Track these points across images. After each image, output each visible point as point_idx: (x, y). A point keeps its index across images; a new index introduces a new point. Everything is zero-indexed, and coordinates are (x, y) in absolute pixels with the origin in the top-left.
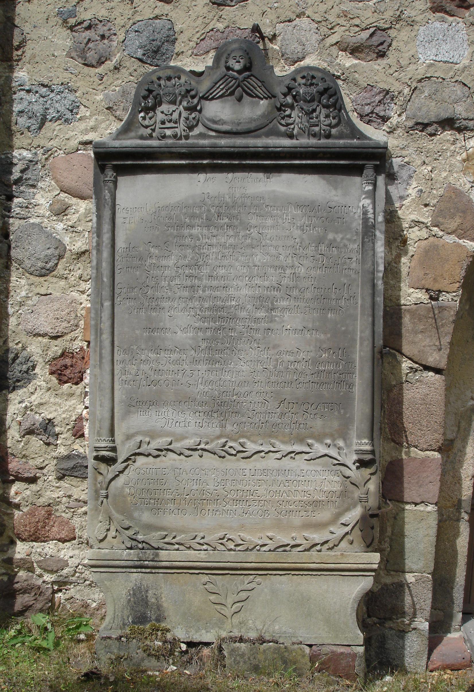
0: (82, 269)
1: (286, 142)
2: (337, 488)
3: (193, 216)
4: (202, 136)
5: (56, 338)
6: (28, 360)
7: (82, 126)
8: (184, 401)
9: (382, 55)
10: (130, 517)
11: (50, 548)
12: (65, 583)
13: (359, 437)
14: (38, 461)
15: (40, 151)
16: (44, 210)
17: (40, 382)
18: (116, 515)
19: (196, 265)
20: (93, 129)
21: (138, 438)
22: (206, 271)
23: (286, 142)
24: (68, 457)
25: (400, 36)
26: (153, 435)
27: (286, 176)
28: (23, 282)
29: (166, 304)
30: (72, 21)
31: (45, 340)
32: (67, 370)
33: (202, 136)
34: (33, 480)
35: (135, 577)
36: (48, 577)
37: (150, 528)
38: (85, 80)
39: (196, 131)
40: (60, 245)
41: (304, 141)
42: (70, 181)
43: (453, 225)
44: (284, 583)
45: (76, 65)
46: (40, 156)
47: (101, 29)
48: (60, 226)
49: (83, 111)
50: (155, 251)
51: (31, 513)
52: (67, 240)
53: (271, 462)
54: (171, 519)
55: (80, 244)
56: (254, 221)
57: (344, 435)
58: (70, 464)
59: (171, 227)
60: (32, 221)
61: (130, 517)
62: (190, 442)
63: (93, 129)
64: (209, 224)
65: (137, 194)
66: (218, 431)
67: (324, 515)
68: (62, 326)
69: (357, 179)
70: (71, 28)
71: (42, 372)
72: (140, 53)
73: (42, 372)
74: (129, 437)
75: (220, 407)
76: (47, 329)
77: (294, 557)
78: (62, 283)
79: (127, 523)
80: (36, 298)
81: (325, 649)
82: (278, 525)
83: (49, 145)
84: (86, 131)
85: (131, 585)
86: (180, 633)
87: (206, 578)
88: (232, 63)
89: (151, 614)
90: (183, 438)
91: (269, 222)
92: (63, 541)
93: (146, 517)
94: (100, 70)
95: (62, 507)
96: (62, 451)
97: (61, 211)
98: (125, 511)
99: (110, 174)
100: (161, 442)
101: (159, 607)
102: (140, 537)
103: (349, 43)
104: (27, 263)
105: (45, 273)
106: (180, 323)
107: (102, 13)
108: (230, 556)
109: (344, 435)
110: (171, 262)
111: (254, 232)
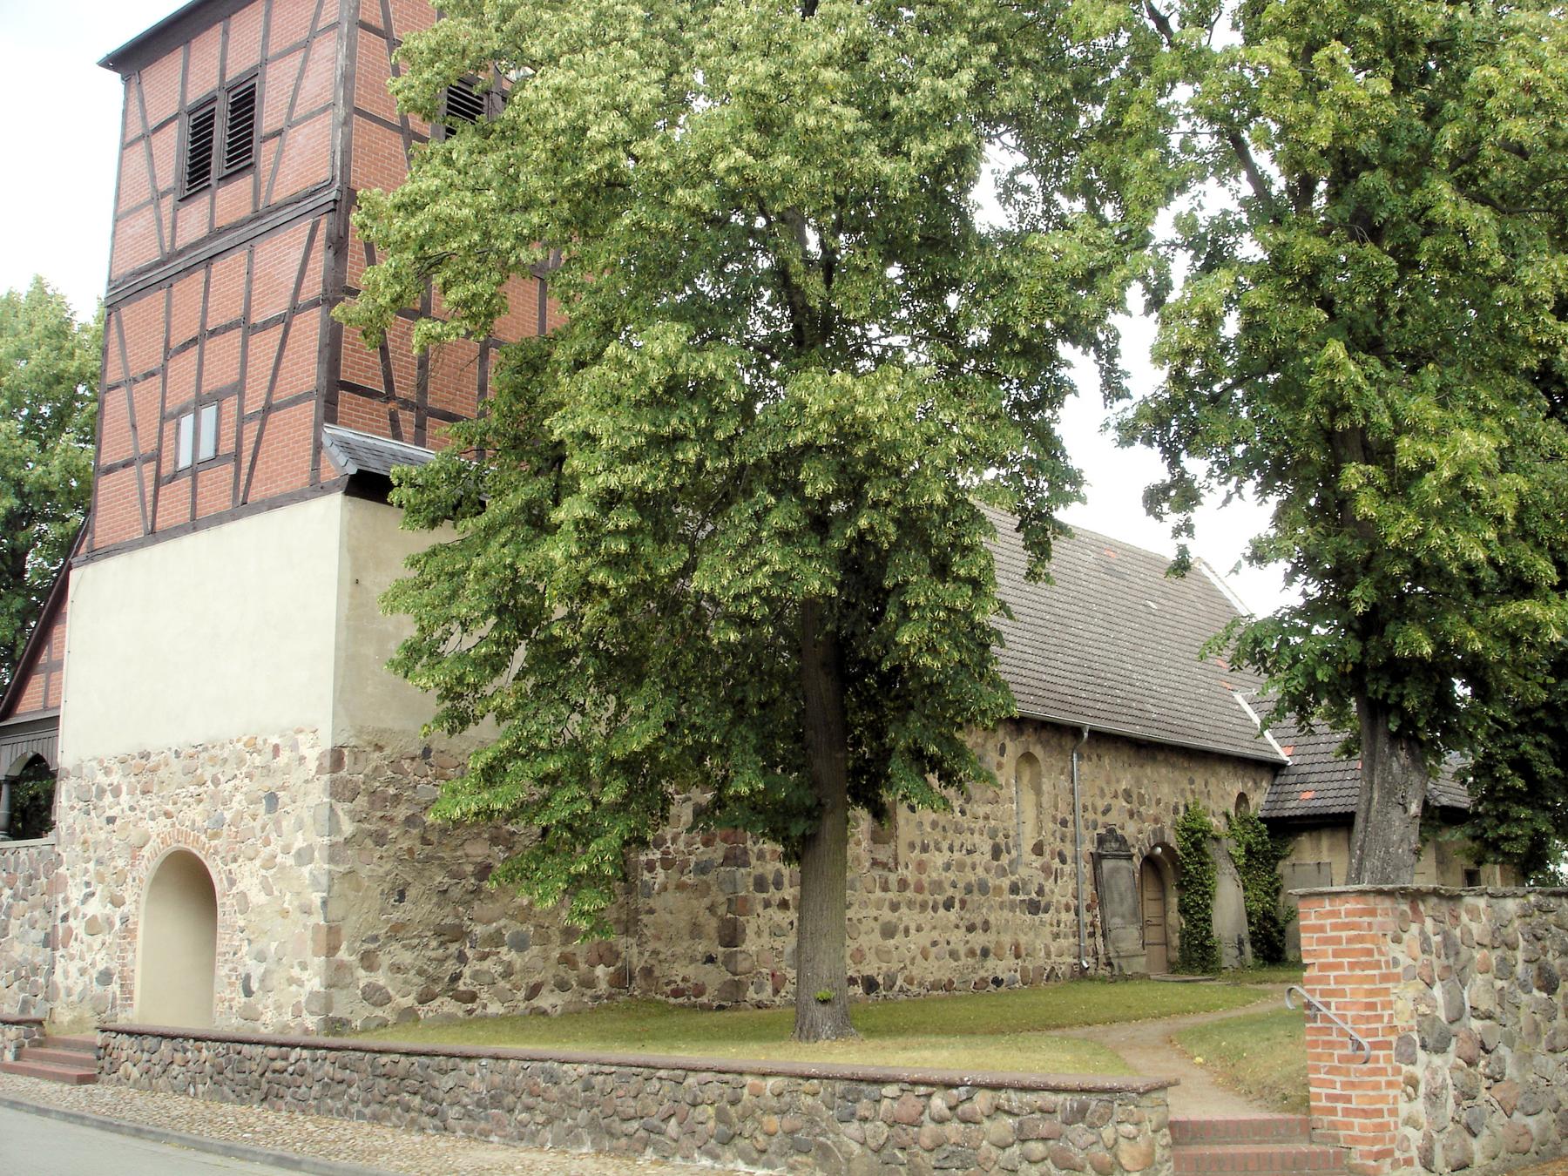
59: (1116, 870)
75: (1123, 917)
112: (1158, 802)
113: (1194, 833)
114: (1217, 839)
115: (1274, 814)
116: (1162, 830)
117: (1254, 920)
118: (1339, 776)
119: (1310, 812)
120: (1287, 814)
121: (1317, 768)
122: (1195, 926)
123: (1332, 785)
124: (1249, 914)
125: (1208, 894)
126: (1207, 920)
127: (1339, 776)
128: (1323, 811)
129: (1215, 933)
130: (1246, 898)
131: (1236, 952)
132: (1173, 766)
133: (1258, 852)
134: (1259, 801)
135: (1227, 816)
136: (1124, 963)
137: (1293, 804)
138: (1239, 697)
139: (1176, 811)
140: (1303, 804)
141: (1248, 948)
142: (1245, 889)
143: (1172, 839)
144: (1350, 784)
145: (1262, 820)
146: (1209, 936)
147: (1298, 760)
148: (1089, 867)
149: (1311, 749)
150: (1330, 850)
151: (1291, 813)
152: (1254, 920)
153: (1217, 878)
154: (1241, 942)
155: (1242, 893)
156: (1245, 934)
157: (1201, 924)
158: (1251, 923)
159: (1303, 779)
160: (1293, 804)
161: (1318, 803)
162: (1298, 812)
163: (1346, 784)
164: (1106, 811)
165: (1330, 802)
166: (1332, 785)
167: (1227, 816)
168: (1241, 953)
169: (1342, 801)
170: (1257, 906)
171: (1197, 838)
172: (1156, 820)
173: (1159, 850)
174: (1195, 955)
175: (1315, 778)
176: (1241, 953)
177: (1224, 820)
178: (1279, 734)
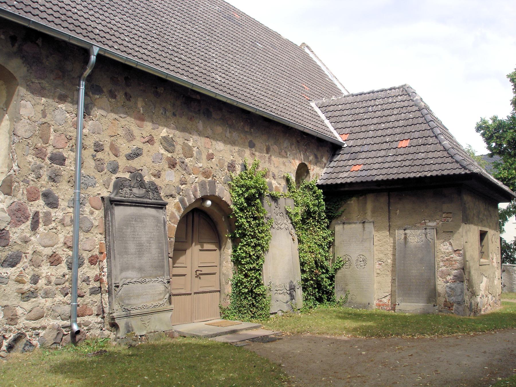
0: (96, 231)
1: (150, 201)
2: (164, 289)
3: (132, 218)
4: (133, 197)
5: (90, 251)
6: (83, 258)
7: (97, 189)
8: (133, 268)
9: (159, 177)
10: (123, 302)
11: (86, 318)
12: (90, 329)
13: (167, 275)
14: (85, 290)
15: (87, 195)
16: (88, 213)
17: (85, 265)
18: (120, 303)
19: (134, 232)
20: (100, 190)
21: (124, 280)
22: (136, 233)
23: (150, 201)
24: (93, 288)
25: (163, 173)
26: (127, 278)
27: (149, 209)
28: (82, 234)
29: (128, 242)
30: (95, 158)
31: (88, 252)
32: (93, 261)
33: (133, 197)
34: (82, 296)
35: (125, 319)
36: (85, 328)
37: (128, 305)
38: (98, 175)
39: (131, 196)
40: (92, 224)
41: (153, 201)
42: (94, 204)
43: (173, 221)
44: (156, 316)
45: (96, 171)
46: (87, 197)
47: (102, 162)
48: (92, 218)
49: (97, 185)
50: (125, 228)
51: (82, 307)
52: (93, 222)
53: (151, 284)
54: (133, 302)
55: (96, 223)
56: (145, 220)
57: (163, 275)
58: (93, 290)
59: (128, 221)
60: (85, 216)
61: (123, 302)
62: (134, 280)
63: (100, 190)
64: (136, 221)
65: (119, 212)
66: (140, 276)
67: (162, 297)
68: (92, 248)
69: (161, 210)
70: (95, 160)
71: (86, 262)
72: (111, 170)
73: (86, 262)
74: (121, 280)
75: (141, 269)
76: (88, 248)
77: (157, 309)
78: (92, 235)
79: (123, 304)
80: (85, 239)
81: (168, 331)
82: (154, 300)
83: (89, 193)
84: (98, 191)
85: (125, 322)
86: (138, 333)
87: (140, 317)
88: (138, 179)
89: (130, 329)
90: (132, 279)
91: (147, 221)
92: (90, 315)
93: (127, 302)
94: (102, 173)
95: (90, 304)
96: (91, 286)
97: (92, 213)
98: (122, 301)
99: (113, 205)
100: (128, 280)
101: (132, 327)
102: (126, 308)
103: (446, 291)
104: (84, 228)
105: (88, 231)
106: (132, 247)
107: (102, 157)
108: (145, 310)
109: (163, 275)
110: (129, 230)
111: (145, 223)
112: (210, 157)
113: (248, 189)
114: (274, 198)
115: (329, 182)
116: (213, 184)
117: (307, 268)
118: (383, 153)
119: (359, 180)
120: (339, 182)
121: (366, 148)
122: (246, 276)
123: (376, 160)
124: (302, 264)
125: (261, 247)
126: (258, 270)
127: (383, 153)
128: (369, 179)
129: (265, 280)
130: (300, 250)
131: (288, 297)
132: (231, 126)
133: (315, 213)
134: (319, 174)
135: (288, 180)
136: (135, 323)
137: (346, 174)
138: (313, 104)
139: (231, 167)
140: (353, 174)
141: (299, 293)
142: (300, 241)
143: (226, 195)
144: (391, 159)
145: (320, 187)
146: (259, 283)
147: (351, 143)
148: (99, 214)
149: (362, 135)
150: (374, 212)
151: (343, 181)
152: (307, 268)
153: (272, 231)
154: (292, 289)
155: (296, 245)
156: (298, 277)
157: (252, 274)
158: (303, 271)
159: (354, 155)
160: (346, 174)
161: (364, 173)
162: (349, 181)
163: (389, 159)
164: (136, 154)
165: (374, 172)
166: (376, 160)
167: (288, 180)
168: (292, 297)
169: (384, 171)
170: (309, 257)
171: (254, 197)
172: (206, 174)
173: (209, 203)
174: (245, 302)
175: (363, 155)
176: (292, 297)
177: (284, 183)
178: (339, 125)
